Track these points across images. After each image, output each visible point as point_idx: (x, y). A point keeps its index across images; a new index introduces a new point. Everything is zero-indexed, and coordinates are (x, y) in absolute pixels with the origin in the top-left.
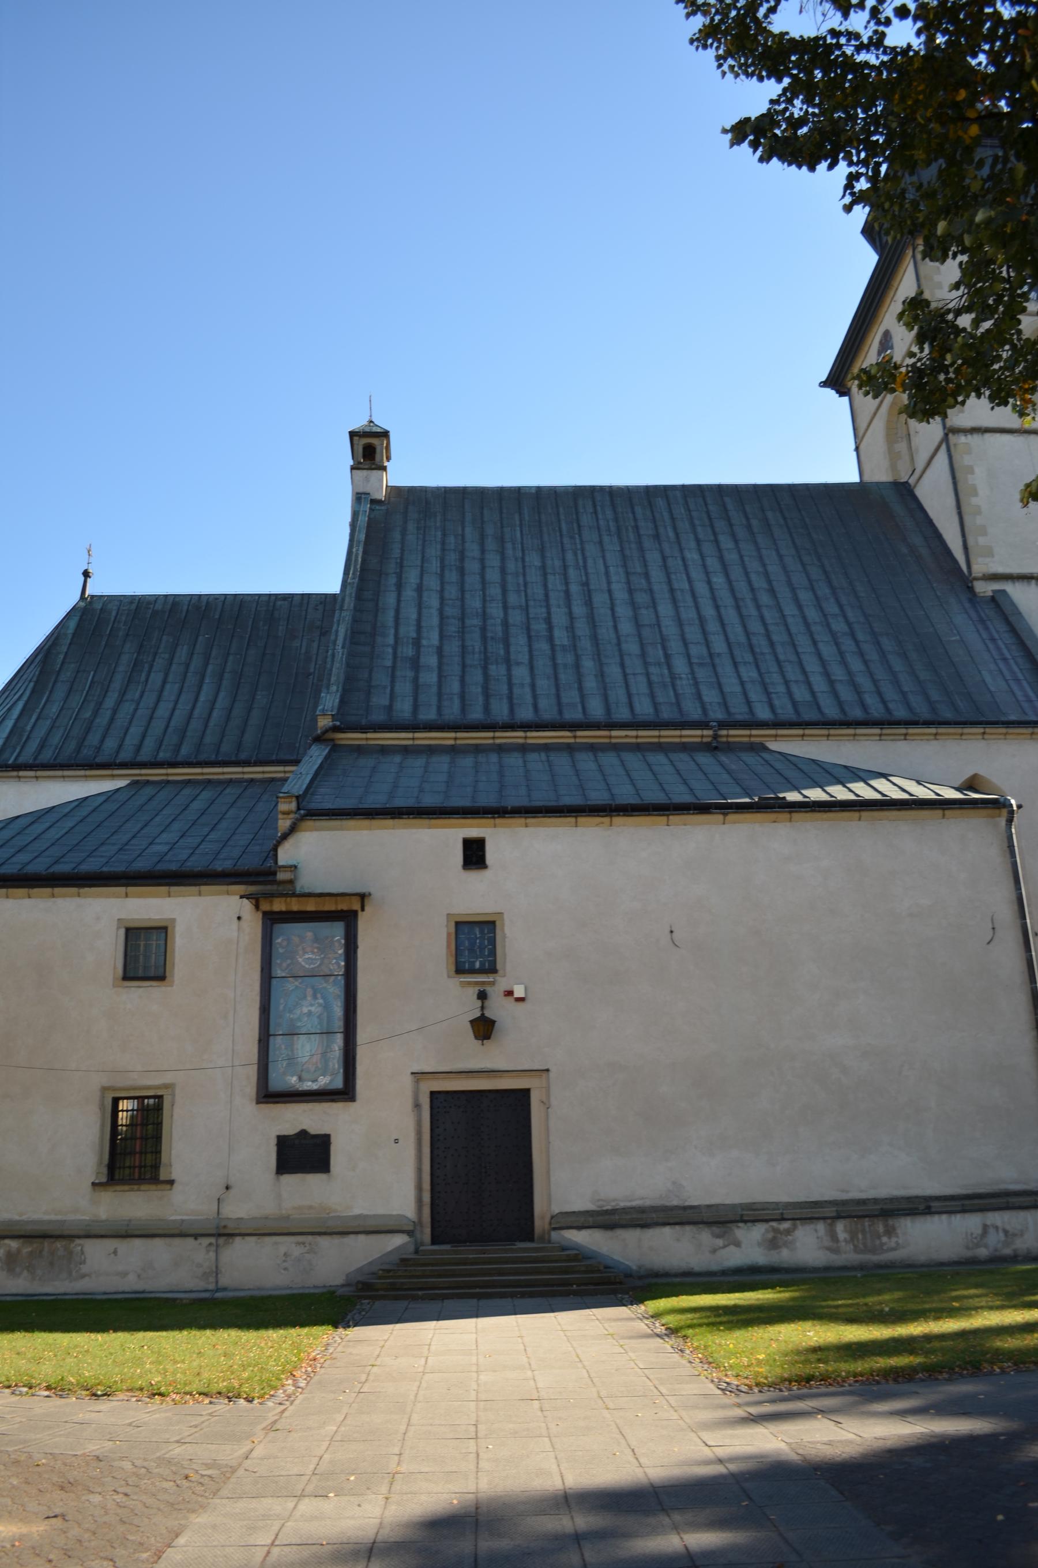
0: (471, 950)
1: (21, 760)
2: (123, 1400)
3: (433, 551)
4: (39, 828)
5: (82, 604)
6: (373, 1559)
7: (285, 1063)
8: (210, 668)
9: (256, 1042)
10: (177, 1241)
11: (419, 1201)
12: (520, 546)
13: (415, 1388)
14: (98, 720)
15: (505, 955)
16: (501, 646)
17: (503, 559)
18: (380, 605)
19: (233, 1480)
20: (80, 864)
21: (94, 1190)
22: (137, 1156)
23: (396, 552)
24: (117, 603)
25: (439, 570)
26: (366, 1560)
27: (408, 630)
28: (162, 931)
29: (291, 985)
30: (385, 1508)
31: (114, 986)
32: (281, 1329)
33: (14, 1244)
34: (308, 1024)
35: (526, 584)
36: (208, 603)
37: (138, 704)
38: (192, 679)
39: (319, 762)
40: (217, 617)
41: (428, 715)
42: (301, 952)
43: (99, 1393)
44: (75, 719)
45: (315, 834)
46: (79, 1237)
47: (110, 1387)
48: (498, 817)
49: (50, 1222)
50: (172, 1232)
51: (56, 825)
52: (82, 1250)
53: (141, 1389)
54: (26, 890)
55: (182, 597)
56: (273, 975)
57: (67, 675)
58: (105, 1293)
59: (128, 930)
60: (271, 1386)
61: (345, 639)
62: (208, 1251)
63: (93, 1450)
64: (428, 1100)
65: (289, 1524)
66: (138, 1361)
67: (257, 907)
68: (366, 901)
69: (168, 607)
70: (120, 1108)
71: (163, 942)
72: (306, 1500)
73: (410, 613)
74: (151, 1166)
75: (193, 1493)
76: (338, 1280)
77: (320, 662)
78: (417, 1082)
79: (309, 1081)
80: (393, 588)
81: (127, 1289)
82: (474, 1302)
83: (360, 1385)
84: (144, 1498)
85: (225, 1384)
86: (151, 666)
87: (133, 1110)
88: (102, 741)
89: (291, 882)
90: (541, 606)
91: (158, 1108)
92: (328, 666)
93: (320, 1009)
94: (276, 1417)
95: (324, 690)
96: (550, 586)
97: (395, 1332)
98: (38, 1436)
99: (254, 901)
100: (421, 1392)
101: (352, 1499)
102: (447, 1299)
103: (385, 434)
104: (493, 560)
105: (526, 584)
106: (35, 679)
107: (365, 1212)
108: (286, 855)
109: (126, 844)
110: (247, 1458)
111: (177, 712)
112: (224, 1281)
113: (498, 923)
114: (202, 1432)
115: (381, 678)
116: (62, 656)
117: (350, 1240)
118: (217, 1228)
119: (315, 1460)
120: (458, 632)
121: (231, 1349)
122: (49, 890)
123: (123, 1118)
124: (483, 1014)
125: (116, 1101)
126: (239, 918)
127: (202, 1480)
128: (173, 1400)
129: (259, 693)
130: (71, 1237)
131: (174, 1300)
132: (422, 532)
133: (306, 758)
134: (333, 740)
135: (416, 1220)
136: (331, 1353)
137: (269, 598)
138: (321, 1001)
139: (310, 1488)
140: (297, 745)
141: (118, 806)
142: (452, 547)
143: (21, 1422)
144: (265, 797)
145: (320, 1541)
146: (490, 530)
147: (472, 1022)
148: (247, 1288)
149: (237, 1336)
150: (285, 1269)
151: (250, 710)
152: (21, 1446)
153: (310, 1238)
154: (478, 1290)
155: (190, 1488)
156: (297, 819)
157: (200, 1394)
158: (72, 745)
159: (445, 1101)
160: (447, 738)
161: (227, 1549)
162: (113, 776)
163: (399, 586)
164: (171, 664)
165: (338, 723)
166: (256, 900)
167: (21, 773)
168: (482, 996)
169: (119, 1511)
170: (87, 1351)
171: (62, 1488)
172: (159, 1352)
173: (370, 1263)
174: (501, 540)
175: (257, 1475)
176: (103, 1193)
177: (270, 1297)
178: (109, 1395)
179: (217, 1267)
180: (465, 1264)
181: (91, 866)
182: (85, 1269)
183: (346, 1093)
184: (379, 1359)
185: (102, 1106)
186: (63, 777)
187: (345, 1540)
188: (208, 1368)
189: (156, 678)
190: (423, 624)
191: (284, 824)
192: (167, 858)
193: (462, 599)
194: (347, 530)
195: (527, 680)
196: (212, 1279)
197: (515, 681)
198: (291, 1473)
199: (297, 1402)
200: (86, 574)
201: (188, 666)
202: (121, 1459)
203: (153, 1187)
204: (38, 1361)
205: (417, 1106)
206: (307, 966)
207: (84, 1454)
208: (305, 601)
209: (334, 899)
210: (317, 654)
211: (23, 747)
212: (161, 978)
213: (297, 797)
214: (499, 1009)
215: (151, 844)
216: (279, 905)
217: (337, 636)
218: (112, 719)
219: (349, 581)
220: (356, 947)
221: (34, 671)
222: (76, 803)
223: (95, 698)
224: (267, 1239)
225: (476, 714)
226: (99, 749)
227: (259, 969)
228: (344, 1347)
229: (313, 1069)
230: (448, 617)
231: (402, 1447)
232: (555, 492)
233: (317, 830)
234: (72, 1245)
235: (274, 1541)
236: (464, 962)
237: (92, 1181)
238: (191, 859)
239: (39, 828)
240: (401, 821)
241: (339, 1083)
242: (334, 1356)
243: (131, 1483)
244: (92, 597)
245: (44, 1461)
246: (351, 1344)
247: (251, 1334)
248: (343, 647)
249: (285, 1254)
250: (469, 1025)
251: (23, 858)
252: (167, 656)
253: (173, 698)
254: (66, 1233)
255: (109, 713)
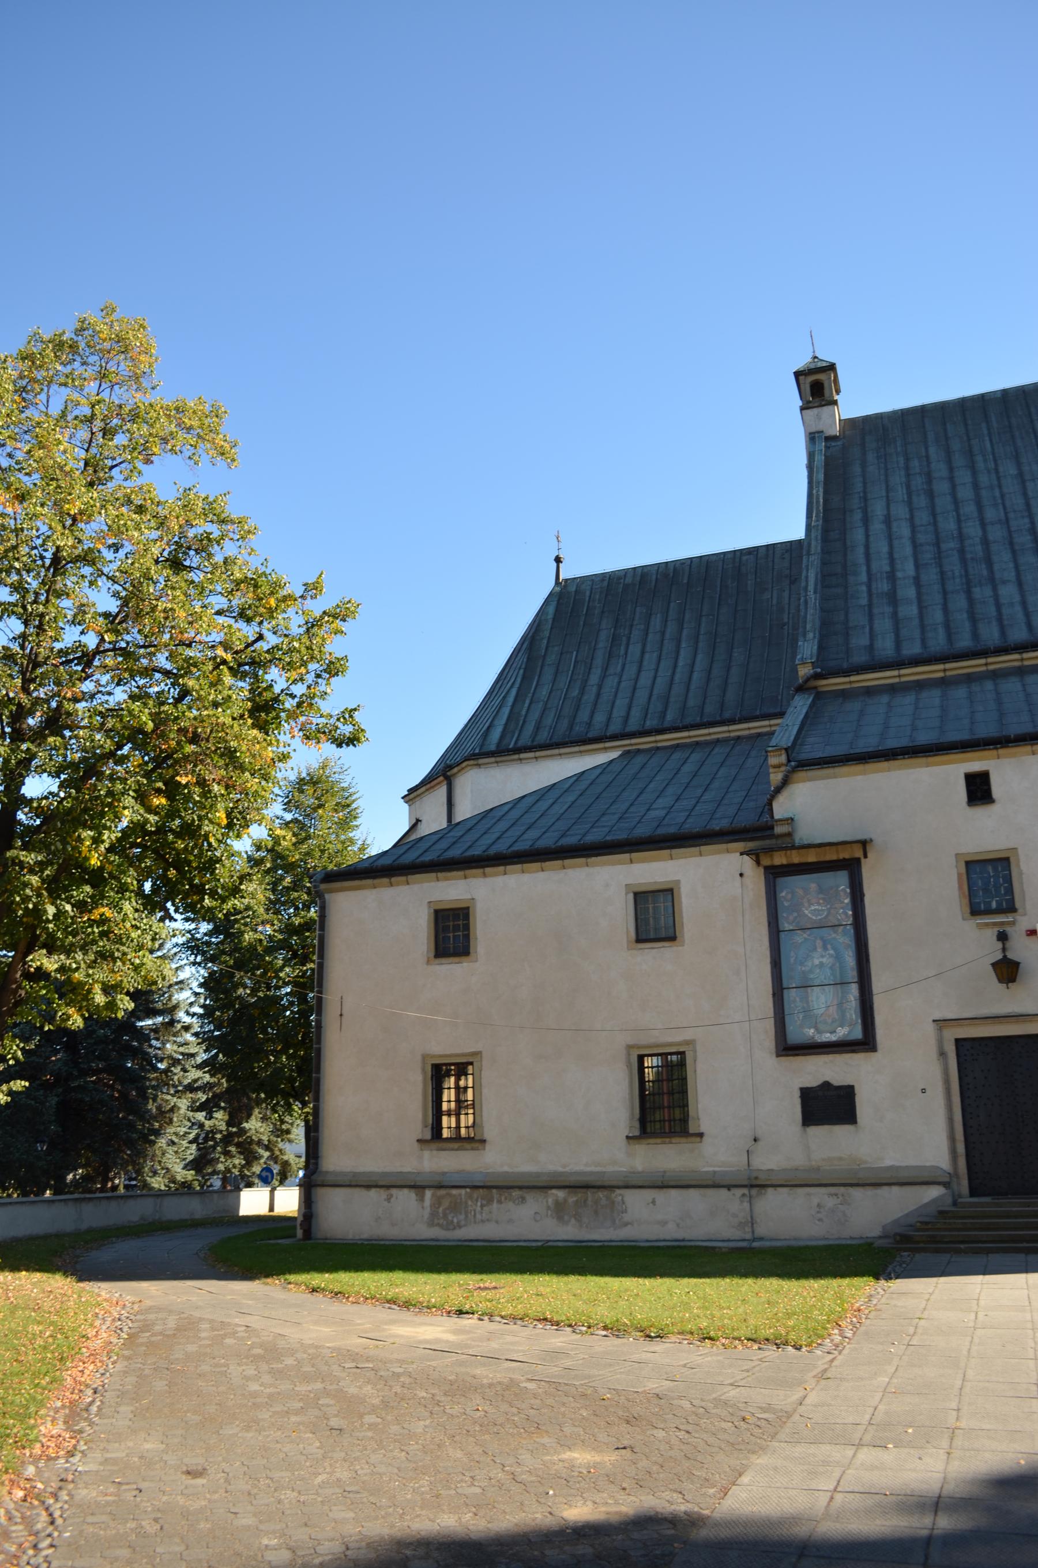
0: (986, 890)
1: (520, 744)
2: (675, 1342)
3: (898, 479)
4: (543, 805)
5: (558, 589)
6: (939, 1513)
7: (801, 1016)
8: (685, 632)
9: (771, 996)
10: (710, 1192)
11: (953, 1152)
12: (991, 457)
13: (967, 1344)
14: (585, 697)
15: (1023, 891)
16: (984, 566)
17: (974, 473)
18: (849, 543)
19: (789, 1425)
20: (584, 835)
21: (629, 1143)
22: (666, 1110)
23: (859, 487)
24: (590, 583)
25: (905, 496)
26: (933, 1513)
27: (881, 565)
28: (668, 893)
29: (800, 938)
30: (947, 1463)
31: (628, 949)
32: (822, 1279)
33: (561, 1194)
34: (819, 976)
35: (1002, 496)
36: (675, 569)
37: (621, 677)
38: (668, 646)
39: (804, 711)
40: (685, 581)
41: (913, 649)
42: (806, 905)
43: (653, 1334)
44: (564, 698)
45: (808, 784)
46: (619, 1187)
47: (662, 1330)
48: (1001, 748)
49: (592, 1173)
50: (705, 1183)
51: (559, 801)
52: (622, 1200)
53: (692, 1333)
54: (539, 864)
55: (649, 568)
56: (781, 929)
57: (551, 659)
58: (648, 1241)
59: (636, 895)
60: (816, 1336)
61: (816, 585)
62: (742, 1202)
63: (653, 1388)
64: (954, 1048)
65: (849, 1471)
66: (687, 1306)
67: (758, 863)
68: (868, 848)
69: (638, 578)
70: (646, 1065)
71: (671, 904)
72: (865, 1449)
73: (881, 547)
74: (680, 1120)
75: (751, 1435)
76: (876, 1232)
77: (792, 611)
78: (940, 1029)
79: (827, 1032)
80: (860, 524)
81: (668, 1237)
82: (1021, 1257)
83: (909, 1337)
84: (705, 1436)
85: (772, 1331)
86: (629, 639)
87: (658, 1066)
88: (592, 716)
89: (789, 835)
90: (1023, 517)
91: (682, 1064)
92: (802, 614)
93: (831, 960)
94: (826, 1366)
95: (801, 638)
96: (1030, 494)
97: (939, 1286)
98: (601, 1372)
99: (754, 857)
100: (974, 1348)
101: (912, 1451)
102: (992, 1253)
103: (832, 367)
104: (964, 476)
105: (1002, 496)
106: (523, 666)
107: (897, 1164)
108: (781, 808)
109: (625, 813)
110: (801, 1404)
111: (659, 680)
112: (761, 1230)
113: (1012, 860)
114: (754, 1376)
115: (858, 618)
116: (545, 641)
117: (884, 1191)
118: (749, 1179)
119: (870, 1410)
120: (935, 558)
121: (774, 1297)
122: (559, 862)
123: (650, 1074)
124: (1005, 956)
125: (641, 1058)
126: (741, 875)
127: (759, 1423)
128: (723, 1345)
129: (735, 650)
130: (612, 1188)
131: (713, 1248)
132: (883, 460)
133: (791, 709)
134: (816, 688)
135: (951, 1171)
136: (876, 1305)
137: (635, 572)
138: (832, 952)
139: (867, 1438)
140: (780, 697)
141: (614, 776)
142: (917, 470)
143: (584, 1358)
144: (753, 753)
145: (883, 1491)
146: (956, 445)
147: (994, 965)
148: (783, 1238)
149: (778, 1285)
150: (820, 1220)
151: (728, 669)
152: (587, 1381)
153: (842, 1189)
154: (1025, 1245)
155: (748, 1430)
156: (789, 772)
157: (749, 1339)
158: (564, 724)
159: (972, 1048)
160: (934, 671)
161: (790, 1491)
162: (606, 749)
163: (866, 521)
164: (647, 634)
165: (819, 670)
166: (756, 855)
167: (522, 756)
168: (1003, 937)
169: (683, 1447)
170: (637, 1295)
171: (628, 1422)
172: (705, 1298)
173: (907, 1215)
174: (970, 454)
175: (813, 1421)
176: (637, 1146)
177: (807, 1247)
178: (662, 1337)
179: (752, 1217)
180: (1008, 1217)
181: (595, 836)
182: (627, 1217)
183: (866, 1043)
184: (926, 1313)
185: (629, 1065)
186: (560, 755)
187: (909, 1493)
188: (753, 1315)
189: (635, 649)
190: (896, 556)
191: (776, 778)
192: (665, 822)
193: (935, 523)
194: (804, 473)
195: (1017, 598)
196: (748, 1229)
197: (1003, 601)
198: (846, 1422)
199: (845, 1352)
200: (558, 560)
201: (663, 633)
202: (680, 1398)
203: (683, 1140)
204: (594, 1302)
205: (942, 1054)
206: (814, 918)
207: (645, 1391)
208: (771, 552)
209: (834, 848)
210: (789, 604)
211: (520, 731)
212: (672, 938)
213: (786, 750)
214: (1022, 949)
215: (648, 810)
216: (779, 859)
217: (807, 581)
218: (598, 695)
219: (813, 524)
220: (862, 895)
221: (522, 658)
222: (575, 778)
223: (581, 676)
224: (801, 1191)
225: (964, 642)
226: (589, 724)
227: (766, 924)
228: (887, 1299)
229: (830, 1021)
230: (921, 545)
231: (959, 1402)
232: (1024, 391)
233: (810, 780)
234: (613, 1195)
235: (836, 1487)
236: (979, 903)
237: (626, 1134)
238: (688, 821)
239: (543, 805)
240: (897, 763)
241: (858, 1034)
242: (878, 1307)
243: (691, 1421)
244: (566, 580)
245: (608, 1396)
246: (894, 1296)
247: (792, 1283)
248: (815, 592)
249: (819, 1205)
250: (990, 968)
251: (533, 834)
252: (642, 627)
253: (653, 666)
254: (607, 1183)
255: (594, 689)
